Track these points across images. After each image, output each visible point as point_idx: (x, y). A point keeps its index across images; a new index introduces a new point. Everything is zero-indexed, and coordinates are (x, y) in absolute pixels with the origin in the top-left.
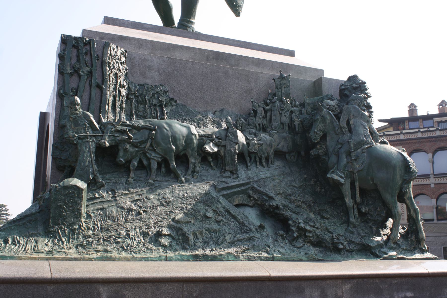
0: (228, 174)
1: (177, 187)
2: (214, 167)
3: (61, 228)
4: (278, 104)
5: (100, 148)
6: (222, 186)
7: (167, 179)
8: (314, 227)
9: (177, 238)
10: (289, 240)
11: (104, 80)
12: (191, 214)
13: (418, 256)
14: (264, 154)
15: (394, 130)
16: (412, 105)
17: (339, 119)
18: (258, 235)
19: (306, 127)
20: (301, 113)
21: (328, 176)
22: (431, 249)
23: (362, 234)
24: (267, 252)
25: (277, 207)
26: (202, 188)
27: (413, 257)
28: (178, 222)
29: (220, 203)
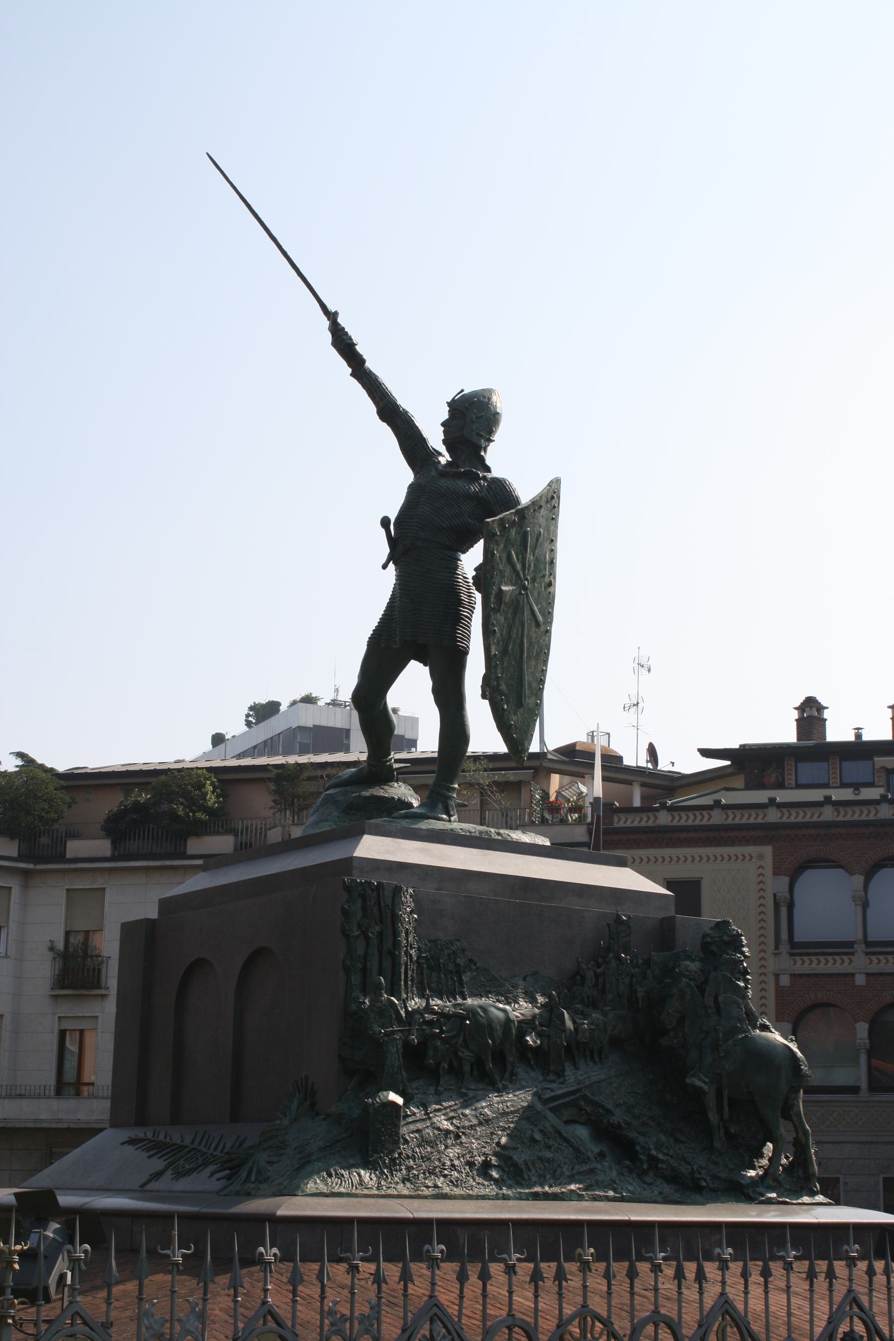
0: (551, 1077)
1: (494, 1098)
3: (380, 1157)
4: (613, 964)
5: (407, 1044)
6: (547, 1096)
7: (481, 1086)
8: (667, 1155)
9: (507, 1169)
11: (396, 944)
12: (516, 1136)
13: (806, 1199)
15: (748, 787)
17: (702, 992)
18: (599, 1166)
21: (688, 1081)
22: (846, 1183)
23: (731, 1166)
24: (615, 1190)
25: (619, 1126)
26: (517, 1099)
27: (800, 1201)
28: (504, 1147)
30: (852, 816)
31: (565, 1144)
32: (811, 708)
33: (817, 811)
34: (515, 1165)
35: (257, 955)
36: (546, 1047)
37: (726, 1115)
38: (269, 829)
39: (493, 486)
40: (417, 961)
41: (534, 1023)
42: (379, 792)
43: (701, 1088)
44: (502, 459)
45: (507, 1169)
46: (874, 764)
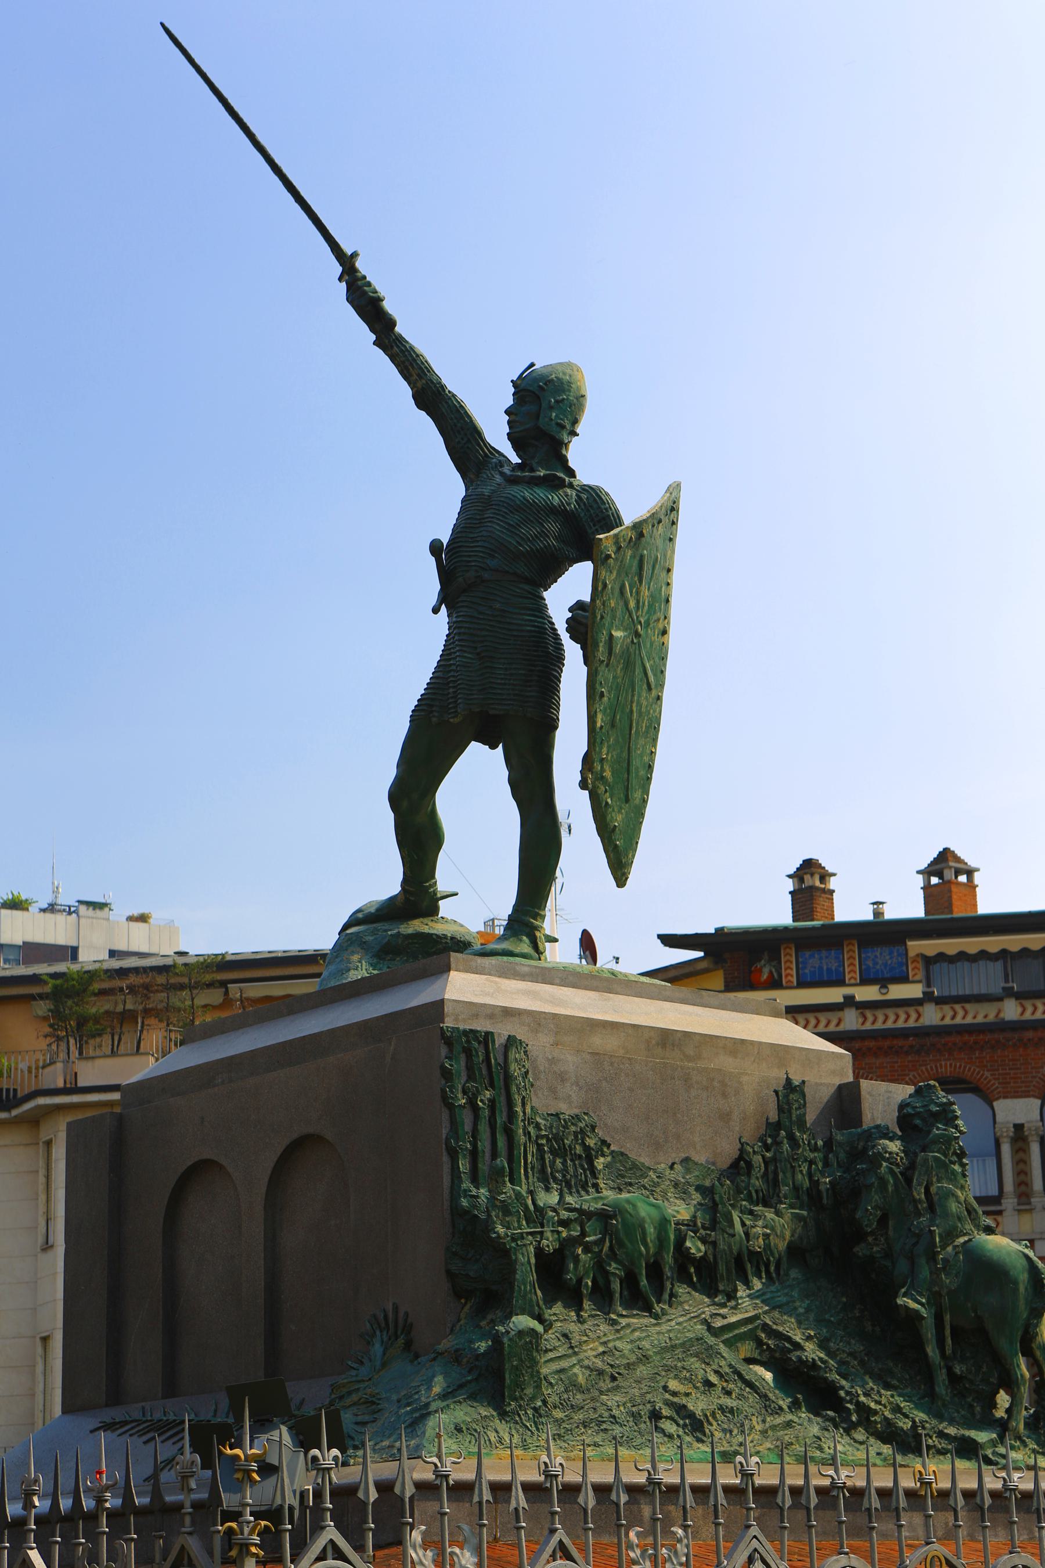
2: (698, 1285)
9: (681, 1422)
10: (844, 1428)
14: (772, 1254)
16: (809, 866)
17: (909, 1181)
19: (848, 1195)
20: (826, 1164)
21: (899, 1301)
29: (723, 1357)
30: (884, 1022)
31: (748, 1389)
32: (812, 875)
33: (834, 1017)
34: (691, 1416)
35: (298, 1148)
36: (711, 1257)
37: (949, 1351)
38: (44, 1067)
39: (584, 496)
40: (536, 1141)
41: (695, 1224)
42: (418, 926)
43: (917, 1311)
44: (588, 459)
45: (681, 1422)
46: (906, 950)
